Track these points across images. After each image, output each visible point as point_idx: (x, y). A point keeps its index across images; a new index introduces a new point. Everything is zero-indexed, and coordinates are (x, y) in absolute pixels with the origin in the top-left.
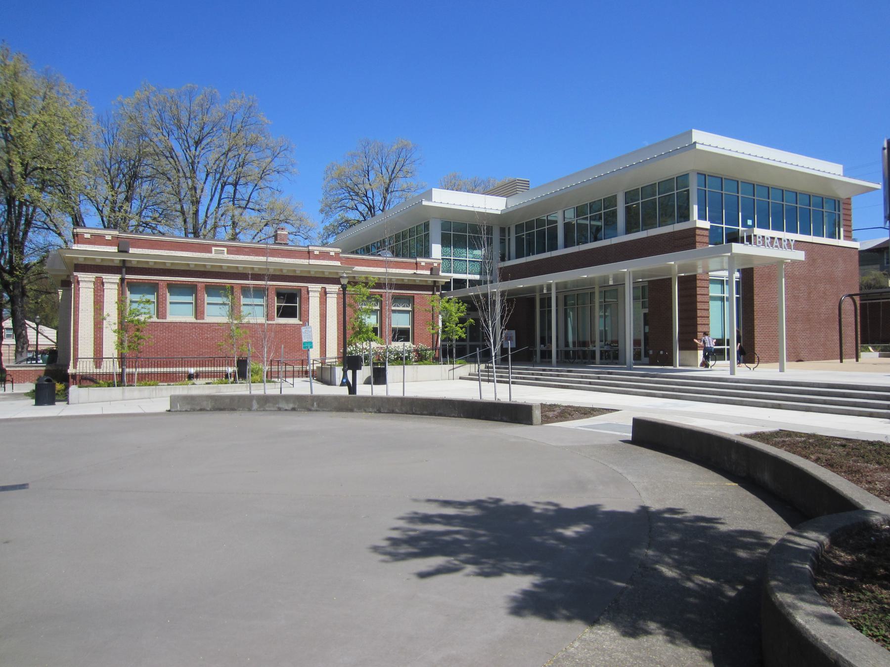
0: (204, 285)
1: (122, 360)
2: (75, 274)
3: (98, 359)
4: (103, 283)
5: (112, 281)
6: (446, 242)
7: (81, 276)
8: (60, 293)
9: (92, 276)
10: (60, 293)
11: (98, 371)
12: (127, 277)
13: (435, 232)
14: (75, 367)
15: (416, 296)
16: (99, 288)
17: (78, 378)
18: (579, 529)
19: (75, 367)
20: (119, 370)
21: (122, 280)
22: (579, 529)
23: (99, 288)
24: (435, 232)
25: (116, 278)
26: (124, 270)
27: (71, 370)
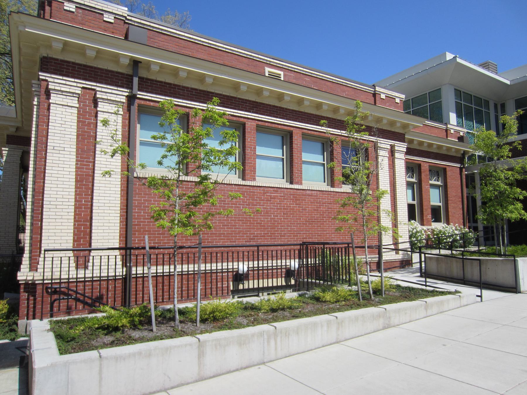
0: (254, 124)
1: (127, 251)
2: (43, 75)
3: (82, 248)
4: (95, 102)
5: (112, 100)
6: (463, 113)
7: (55, 82)
8: (5, 153)
9: (75, 85)
10: (5, 153)
11: (81, 274)
12: (141, 95)
13: (449, 100)
14: (33, 267)
15: (448, 168)
16: (89, 107)
17: (39, 289)
18: (199, 284)
19: (33, 267)
20: (120, 271)
21: (131, 99)
22: (199, 284)
23: (89, 107)
24: (449, 100)
25: (121, 95)
26: (136, 80)
27: (24, 274)
